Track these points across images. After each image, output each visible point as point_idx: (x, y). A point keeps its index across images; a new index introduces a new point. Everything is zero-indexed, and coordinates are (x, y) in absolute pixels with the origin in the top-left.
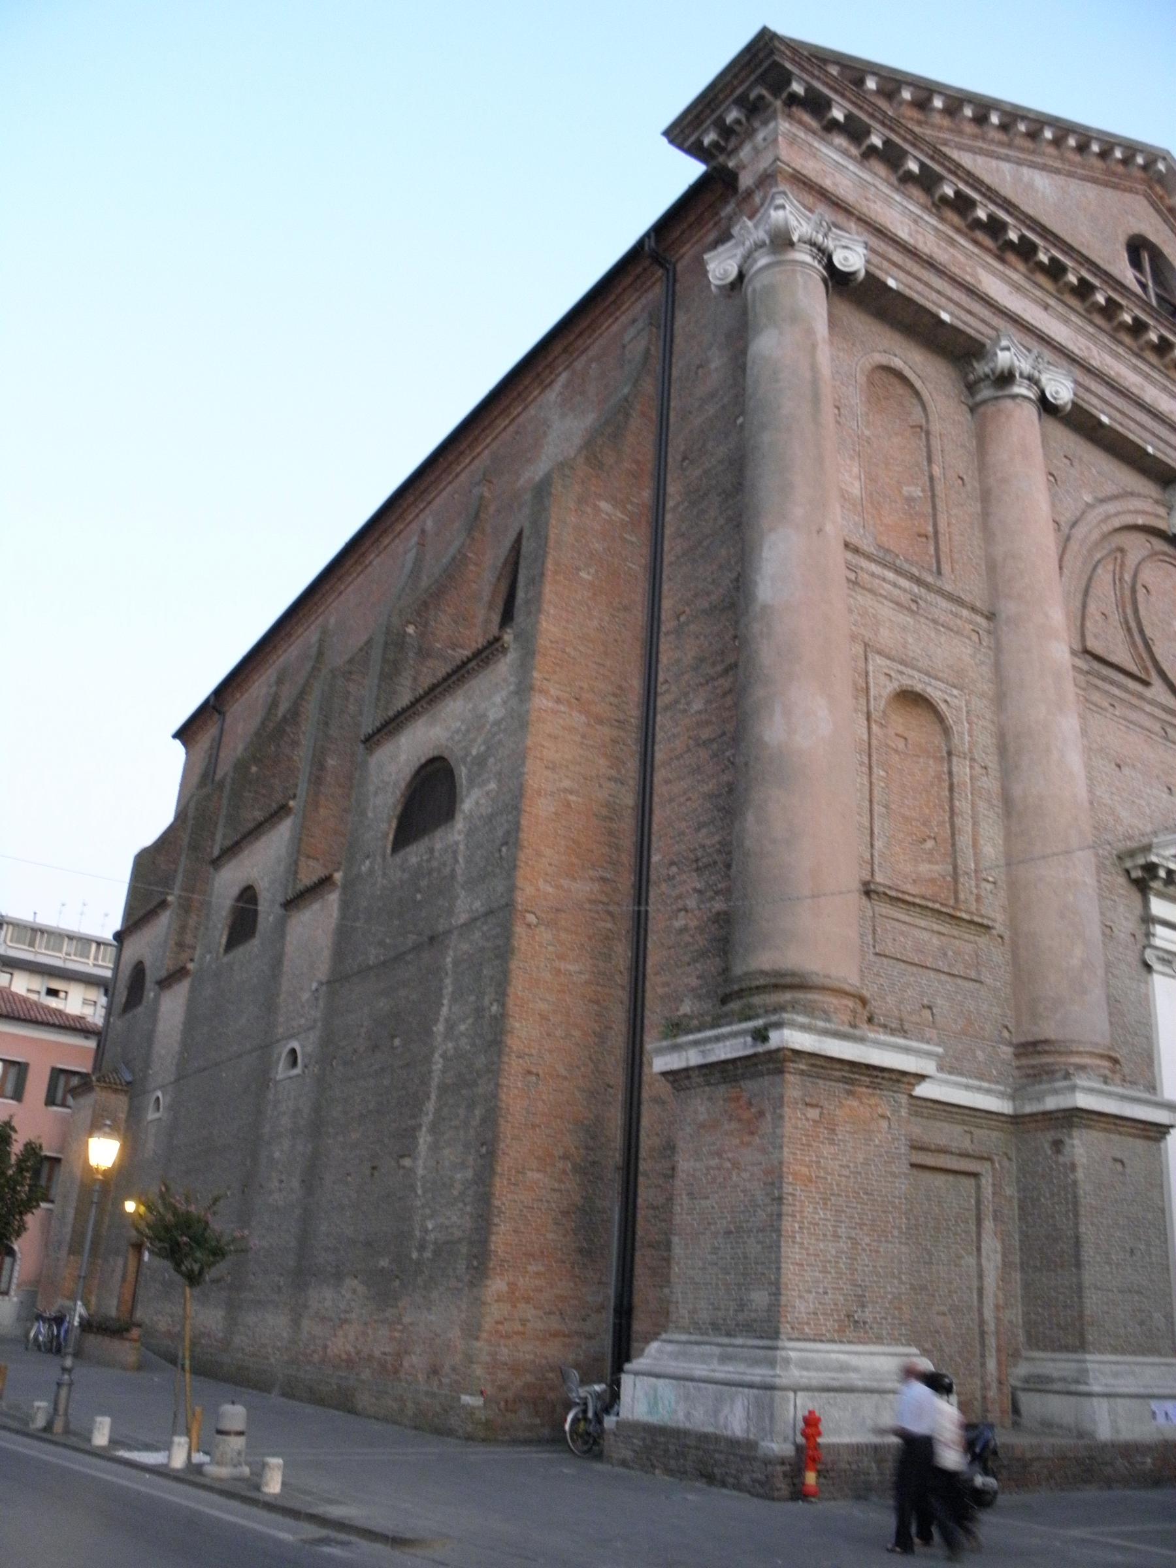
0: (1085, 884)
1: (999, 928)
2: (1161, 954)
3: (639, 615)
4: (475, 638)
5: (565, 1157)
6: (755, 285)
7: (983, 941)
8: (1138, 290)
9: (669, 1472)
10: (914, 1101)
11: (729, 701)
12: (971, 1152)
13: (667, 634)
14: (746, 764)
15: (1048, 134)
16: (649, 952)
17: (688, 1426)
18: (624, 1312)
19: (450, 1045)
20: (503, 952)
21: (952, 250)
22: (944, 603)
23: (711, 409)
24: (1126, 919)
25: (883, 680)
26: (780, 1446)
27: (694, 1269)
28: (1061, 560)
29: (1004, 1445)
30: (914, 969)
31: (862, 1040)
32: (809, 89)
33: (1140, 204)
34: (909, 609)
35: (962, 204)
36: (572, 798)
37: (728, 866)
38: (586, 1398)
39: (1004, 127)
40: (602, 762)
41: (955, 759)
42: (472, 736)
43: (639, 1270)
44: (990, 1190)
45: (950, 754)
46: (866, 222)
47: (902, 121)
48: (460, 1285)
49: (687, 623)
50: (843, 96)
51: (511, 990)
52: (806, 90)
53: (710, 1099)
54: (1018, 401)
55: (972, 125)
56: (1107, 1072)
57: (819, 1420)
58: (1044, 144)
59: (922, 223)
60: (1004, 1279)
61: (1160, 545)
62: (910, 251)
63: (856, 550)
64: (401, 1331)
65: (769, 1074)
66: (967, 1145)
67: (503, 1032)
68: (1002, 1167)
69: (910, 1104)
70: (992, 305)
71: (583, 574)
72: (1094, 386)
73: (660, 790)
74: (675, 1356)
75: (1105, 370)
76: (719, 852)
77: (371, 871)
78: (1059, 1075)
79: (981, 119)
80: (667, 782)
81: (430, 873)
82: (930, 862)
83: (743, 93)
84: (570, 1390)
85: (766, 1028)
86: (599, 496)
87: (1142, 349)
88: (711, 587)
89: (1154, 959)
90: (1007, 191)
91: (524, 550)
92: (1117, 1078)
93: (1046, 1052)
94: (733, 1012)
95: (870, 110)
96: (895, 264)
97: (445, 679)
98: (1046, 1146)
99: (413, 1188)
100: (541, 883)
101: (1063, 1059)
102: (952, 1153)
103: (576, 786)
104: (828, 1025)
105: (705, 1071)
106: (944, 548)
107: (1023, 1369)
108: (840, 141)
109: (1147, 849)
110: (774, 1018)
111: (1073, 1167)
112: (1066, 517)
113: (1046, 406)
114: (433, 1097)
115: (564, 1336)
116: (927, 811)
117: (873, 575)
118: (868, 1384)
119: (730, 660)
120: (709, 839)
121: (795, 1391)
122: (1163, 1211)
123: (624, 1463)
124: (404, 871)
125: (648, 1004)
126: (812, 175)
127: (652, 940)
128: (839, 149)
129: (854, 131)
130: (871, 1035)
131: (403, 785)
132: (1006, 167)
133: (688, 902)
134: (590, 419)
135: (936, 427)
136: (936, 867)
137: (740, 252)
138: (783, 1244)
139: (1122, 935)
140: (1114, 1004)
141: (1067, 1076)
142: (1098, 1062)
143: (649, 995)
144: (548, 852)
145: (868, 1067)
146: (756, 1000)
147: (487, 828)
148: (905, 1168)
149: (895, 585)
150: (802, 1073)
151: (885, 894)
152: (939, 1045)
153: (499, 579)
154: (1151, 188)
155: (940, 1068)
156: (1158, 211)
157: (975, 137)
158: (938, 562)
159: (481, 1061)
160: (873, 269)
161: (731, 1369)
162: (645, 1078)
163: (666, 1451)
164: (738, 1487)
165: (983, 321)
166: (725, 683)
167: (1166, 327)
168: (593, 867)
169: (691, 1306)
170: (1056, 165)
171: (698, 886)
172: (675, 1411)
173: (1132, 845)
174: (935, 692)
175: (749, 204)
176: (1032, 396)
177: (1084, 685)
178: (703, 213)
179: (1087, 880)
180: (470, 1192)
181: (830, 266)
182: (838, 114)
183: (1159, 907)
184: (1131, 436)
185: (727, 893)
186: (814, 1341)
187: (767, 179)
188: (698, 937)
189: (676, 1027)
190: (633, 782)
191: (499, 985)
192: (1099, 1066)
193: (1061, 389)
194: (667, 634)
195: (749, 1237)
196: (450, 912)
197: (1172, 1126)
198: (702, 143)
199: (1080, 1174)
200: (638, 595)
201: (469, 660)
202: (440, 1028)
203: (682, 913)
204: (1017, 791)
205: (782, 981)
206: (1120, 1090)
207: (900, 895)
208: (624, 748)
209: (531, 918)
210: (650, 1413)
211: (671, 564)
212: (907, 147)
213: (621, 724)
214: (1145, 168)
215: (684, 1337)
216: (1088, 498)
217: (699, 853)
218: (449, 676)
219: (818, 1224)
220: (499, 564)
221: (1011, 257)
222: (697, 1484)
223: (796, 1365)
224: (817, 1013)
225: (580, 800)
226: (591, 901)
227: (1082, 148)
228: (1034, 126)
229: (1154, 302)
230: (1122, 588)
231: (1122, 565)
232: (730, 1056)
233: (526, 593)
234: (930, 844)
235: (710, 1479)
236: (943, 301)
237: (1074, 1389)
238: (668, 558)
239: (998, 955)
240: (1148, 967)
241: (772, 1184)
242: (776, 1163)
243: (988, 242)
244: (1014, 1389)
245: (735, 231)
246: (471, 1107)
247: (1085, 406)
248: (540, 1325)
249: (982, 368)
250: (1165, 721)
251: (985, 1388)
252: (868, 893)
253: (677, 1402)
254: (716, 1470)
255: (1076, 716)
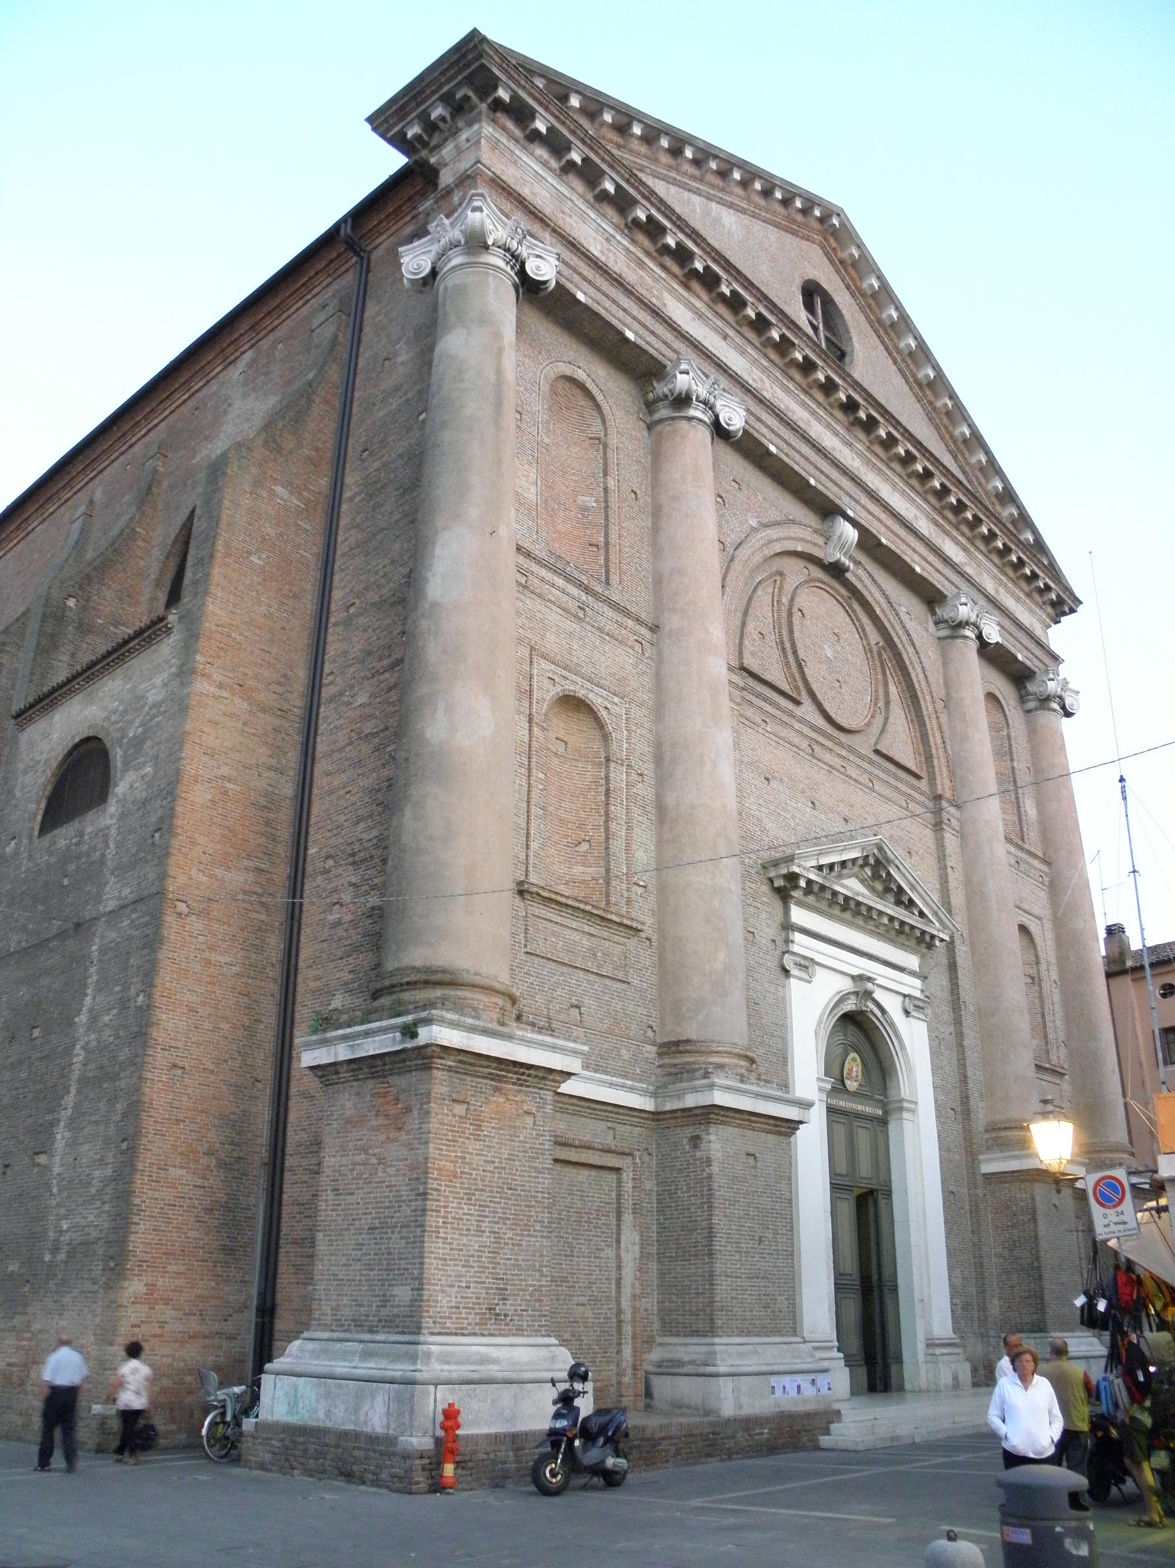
0: (730, 890)
1: (648, 931)
2: (798, 959)
3: (309, 605)
4: (138, 616)
5: (209, 1153)
6: (446, 284)
7: (632, 943)
8: (810, 332)
9: (309, 1473)
10: (557, 1098)
11: (394, 696)
12: (613, 1148)
13: (335, 625)
14: (407, 760)
15: (737, 175)
16: (302, 945)
17: (328, 1424)
18: (267, 1311)
19: (93, 1037)
20: (152, 941)
21: (641, 272)
22: (610, 613)
23: (395, 403)
24: (769, 926)
25: (547, 684)
26: (420, 1441)
27: (338, 1265)
28: (724, 579)
29: (635, 1427)
30: (565, 969)
31: (510, 1037)
32: (515, 97)
33: (815, 253)
34: (576, 617)
35: (652, 229)
36: (229, 786)
37: (384, 861)
38: (224, 1400)
39: (696, 162)
40: (263, 750)
41: (612, 765)
42: (128, 718)
43: (282, 1268)
44: (630, 1185)
45: (608, 760)
46: (560, 235)
47: (603, 142)
48: (96, 1287)
49: (357, 615)
50: (546, 109)
51: (158, 981)
52: (511, 98)
53: (358, 1094)
54: (694, 423)
55: (668, 156)
56: (743, 1071)
57: (458, 1412)
58: (733, 184)
59: (613, 242)
60: (641, 1270)
61: (817, 573)
62: (600, 268)
63: (528, 555)
64: (29, 1340)
65: (416, 1070)
66: (609, 1141)
67: (149, 1024)
68: (643, 1163)
69: (555, 1101)
70: (675, 329)
71: (254, 558)
72: (764, 416)
73: (321, 782)
74: (314, 1354)
75: (776, 402)
76: (376, 846)
77: (16, 853)
78: (698, 1074)
79: (676, 152)
80: (328, 774)
81: (78, 858)
82: (584, 865)
83: (449, 90)
84: (208, 1394)
85: (416, 1024)
86: (276, 481)
87: (810, 387)
88: (383, 581)
89: (792, 964)
90: (696, 223)
91: (194, 530)
92: (753, 1076)
93: (688, 1052)
94: (383, 1008)
95: (572, 127)
96: (585, 279)
97: (104, 657)
98: (685, 1141)
99: (48, 1185)
100: (194, 872)
101: (703, 1059)
102: (594, 1148)
103: (234, 774)
104: (477, 1023)
105: (354, 1066)
106: (614, 559)
107: (656, 1355)
108: (541, 152)
109: (790, 859)
110: (423, 1014)
111: (709, 1162)
112: (731, 539)
113: (719, 431)
114: (73, 1090)
115: (205, 1337)
116: (583, 815)
117: (543, 580)
118: (508, 1375)
119: (397, 655)
120: (366, 833)
121: (436, 1385)
122: (790, 1201)
123: (262, 1466)
124: (50, 855)
125: (299, 998)
126: (511, 182)
127: (306, 932)
128: (539, 160)
129: (555, 144)
130: (520, 1033)
131: (54, 764)
132: (696, 199)
133: (342, 895)
134: (273, 401)
135: (613, 441)
136: (589, 870)
137: (435, 248)
138: (426, 1239)
139: (763, 941)
140: (752, 1006)
141: (706, 1075)
142: (736, 1061)
143: (300, 988)
144: (202, 840)
145: (515, 1063)
146: (407, 996)
147: (140, 813)
148: (549, 1164)
149: (564, 592)
150: (450, 1069)
151: (538, 894)
152: (585, 1044)
153: (167, 558)
154: (825, 239)
155: (586, 1067)
156: (832, 262)
157: (670, 168)
158: (607, 572)
159: (124, 1054)
160: (563, 281)
161: (372, 1365)
162: (293, 1073)
163: (306, 1451)
164: (377, 1483)
165: (665, 343)
166: (390, 678)
167: (833, 369)
168: (249, 857)
169: (334, 1304)
170: (742, 205)
171: (354, 880)
172: (315, 1411)
173: (776, 855)
174: (596, 698)
175: (448, 203)
176: (706, 419)
177: (739, 700)
178: (400, 207)
179: (733, 888)
180: (108, 1190)
181: (522, 272)
182: (541, 126)
183: (798, 915)
184: (796, 467)
185: (381, 888)
186: (456, 1334)
187: (466, 180)
188: (352, 932)
189: (326, 1022)
190: (293, 773)
191: (146, 975)
192: (736, 1066)
193: (734, 416)
194: (335, 625)
195: (393, 1232)
196: (98, 898)
197: (801, 1122)
198: (406, 134)
199: (715, 1169)
200: (309, 585)
201: (131, 639)
202: (83, 1018)
203: (337, 907)
204: (670, 799)
205: (433, 978)
206: (755, 1088)
207: (554, 896)
208: (287, 738)
209: (182, 907)
210: (289, 1413)
211: (343, 555)
212: (604, 167)
213: (283, 713)
214: (822, 220)
215: (326, 1335)
216: (753, 522)
217: (357, 847)
218: (109, 654)
219: (462, 1219)
220: (169, 541)
221: (695, 285)
222: (336, 1483)
223: (437, 1360)
224: (466, 1010)
225: (238, 788)
226: (245, 892)
227: (767, 193)
228: (725, 166)
229: (824, 345)
230: (779, 610)
231: (781, 588)
232: (378, 1052)
233: (194, 574)
234: (584, 847)
235: (349, 1476)
236: (629, 320)
237: (703, 1372)
238: (341, 549)
239: (646, 958)
240: (786, 972)
241: (418, 1179)
242: (421, 1159)
243: (675, 268)
244: (648, 1373)
245: (431, 227)
246: (112, 1101)
247: (756, 434)
248: (178, 1327)
249: (661, 388)
250: (811, 739)
251: (620, 1374)
252: (521, 893)
253: (317, 1401)
254: (355, 1468)
255: (730, 730)
